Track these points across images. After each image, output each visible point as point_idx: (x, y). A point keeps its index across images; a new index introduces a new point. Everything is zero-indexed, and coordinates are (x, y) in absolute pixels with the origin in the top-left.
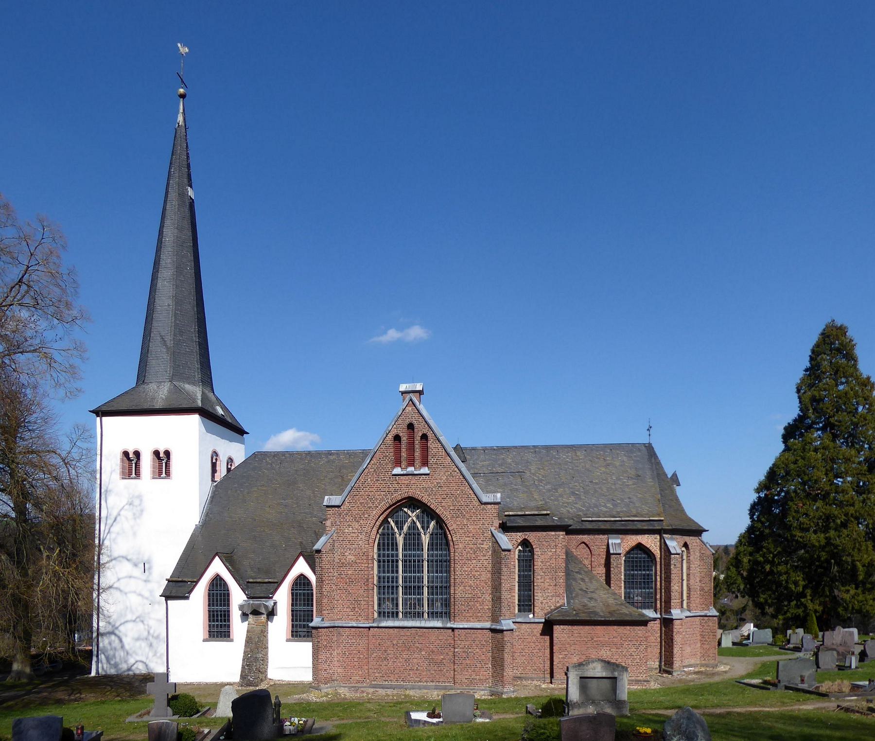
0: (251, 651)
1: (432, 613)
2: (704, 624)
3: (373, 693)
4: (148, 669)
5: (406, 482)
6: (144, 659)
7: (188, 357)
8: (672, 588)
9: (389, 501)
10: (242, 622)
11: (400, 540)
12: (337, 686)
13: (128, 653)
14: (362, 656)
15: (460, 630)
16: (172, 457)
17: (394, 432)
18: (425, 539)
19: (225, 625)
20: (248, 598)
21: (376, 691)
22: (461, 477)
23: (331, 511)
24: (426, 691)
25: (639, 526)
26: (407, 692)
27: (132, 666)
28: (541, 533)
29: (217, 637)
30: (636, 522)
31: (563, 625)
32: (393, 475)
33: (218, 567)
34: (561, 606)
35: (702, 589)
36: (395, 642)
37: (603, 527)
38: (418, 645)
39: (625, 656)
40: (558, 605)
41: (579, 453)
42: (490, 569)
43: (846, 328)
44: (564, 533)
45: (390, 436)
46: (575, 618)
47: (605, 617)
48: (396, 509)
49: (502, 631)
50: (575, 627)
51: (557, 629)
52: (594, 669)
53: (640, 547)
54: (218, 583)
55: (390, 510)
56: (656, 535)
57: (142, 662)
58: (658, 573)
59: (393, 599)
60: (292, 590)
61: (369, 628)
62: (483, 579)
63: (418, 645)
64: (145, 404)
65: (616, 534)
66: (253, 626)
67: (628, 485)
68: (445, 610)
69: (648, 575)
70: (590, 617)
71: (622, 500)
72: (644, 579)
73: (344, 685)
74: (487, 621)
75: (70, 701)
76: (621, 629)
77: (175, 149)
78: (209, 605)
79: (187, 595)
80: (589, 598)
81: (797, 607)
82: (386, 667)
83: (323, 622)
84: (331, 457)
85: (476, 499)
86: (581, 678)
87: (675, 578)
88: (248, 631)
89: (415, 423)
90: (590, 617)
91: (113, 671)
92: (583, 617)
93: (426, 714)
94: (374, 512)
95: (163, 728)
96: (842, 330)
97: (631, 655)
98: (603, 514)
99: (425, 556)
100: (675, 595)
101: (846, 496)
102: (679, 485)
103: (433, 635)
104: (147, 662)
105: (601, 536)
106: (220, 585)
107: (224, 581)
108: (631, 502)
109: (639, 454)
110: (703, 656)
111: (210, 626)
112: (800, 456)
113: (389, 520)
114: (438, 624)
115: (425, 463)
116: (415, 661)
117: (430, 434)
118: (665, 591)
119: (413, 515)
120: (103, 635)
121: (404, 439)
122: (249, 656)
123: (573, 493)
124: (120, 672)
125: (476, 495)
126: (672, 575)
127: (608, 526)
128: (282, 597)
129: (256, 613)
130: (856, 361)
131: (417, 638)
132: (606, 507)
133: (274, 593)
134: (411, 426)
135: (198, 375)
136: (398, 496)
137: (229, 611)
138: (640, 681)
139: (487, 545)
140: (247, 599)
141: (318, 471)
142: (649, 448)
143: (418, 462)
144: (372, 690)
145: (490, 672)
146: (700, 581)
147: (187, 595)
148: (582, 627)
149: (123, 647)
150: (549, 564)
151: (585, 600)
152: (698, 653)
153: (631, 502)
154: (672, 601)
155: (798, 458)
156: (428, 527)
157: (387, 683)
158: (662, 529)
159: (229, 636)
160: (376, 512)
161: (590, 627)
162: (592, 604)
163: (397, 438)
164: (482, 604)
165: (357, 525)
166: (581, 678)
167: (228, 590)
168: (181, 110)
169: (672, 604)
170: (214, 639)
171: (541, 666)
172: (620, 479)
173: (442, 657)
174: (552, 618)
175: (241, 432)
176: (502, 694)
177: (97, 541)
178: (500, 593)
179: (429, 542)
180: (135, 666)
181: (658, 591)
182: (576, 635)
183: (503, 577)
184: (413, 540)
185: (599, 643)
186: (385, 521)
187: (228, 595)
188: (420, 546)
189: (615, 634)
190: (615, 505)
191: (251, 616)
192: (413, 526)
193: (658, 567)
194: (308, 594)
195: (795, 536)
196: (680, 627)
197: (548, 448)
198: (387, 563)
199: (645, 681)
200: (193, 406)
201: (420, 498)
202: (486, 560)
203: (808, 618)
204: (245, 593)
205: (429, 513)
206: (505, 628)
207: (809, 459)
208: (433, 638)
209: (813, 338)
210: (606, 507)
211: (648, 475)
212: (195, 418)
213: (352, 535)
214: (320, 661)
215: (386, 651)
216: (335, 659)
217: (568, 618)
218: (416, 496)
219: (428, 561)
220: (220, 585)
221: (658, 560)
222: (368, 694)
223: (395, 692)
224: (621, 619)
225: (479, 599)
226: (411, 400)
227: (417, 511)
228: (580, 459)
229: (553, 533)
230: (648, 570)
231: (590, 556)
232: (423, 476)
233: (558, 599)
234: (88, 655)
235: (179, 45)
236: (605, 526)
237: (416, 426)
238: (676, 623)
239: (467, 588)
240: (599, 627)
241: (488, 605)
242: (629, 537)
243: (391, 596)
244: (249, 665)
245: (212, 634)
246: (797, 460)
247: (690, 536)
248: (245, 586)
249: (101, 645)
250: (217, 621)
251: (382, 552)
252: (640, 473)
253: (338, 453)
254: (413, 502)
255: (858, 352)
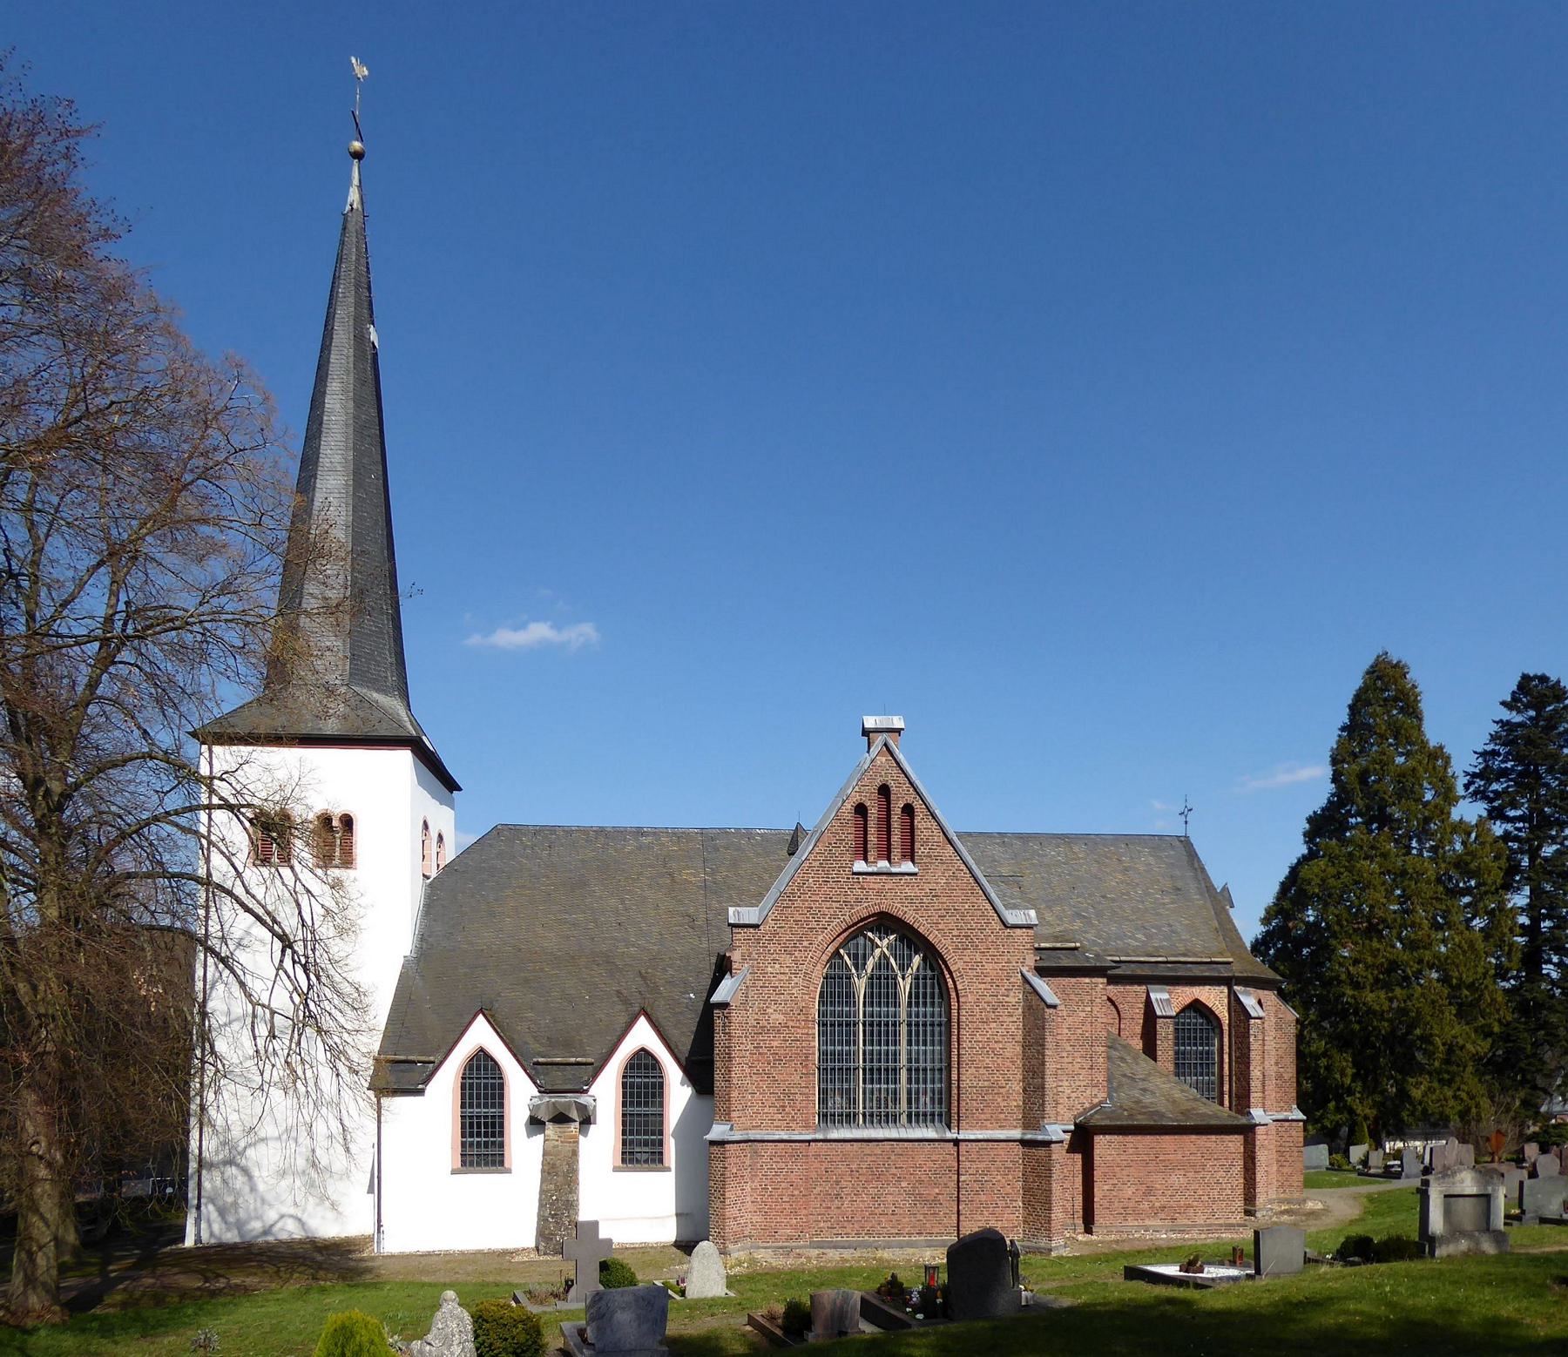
0: (558, 1189)
1: (825, 1115)
2: (1283, 1134)
3: (818, 1257)
4: (305, 1230)
5: (876, 886)
6: (292, 1211)
7: (374, 641)
8: (1252, 1074)
9: (847, 918)
10: (530, 1134)
11: (861, 985)
12: (751, 1247)
13: (263, 1201)
14: (796, 1192)
15: (969, 1144)
16: (358, 827)
17: (856, 799)
18: (905, 986)
19: (493, 1143)
20: (540, 1092)
21: (823, 1254)
22: (972, 880)
23: (741, 935)
24: (911, 1251)
25: (1197, 971)
26: (879, 1254)
27: (272, 1226)
28: (1067, 979)
29: (479, 1164)
30: (1189, 966)
31: (1110, 1134)
32: (854, 874)
33: (481, 1035)
34: (1101, 1102)
35: (1279, 1077)
36: (854, 1167)
37: (1139, 972)
38: (894, 1171)
39: (1208, 1184)
40: (1096, 1101)
41: (1076, 849)
42: (1019, 1038)
43: (1405, 666)
44: (1105, 980)
45: (849, 806)
46: (1130, 1123)
47: (1177, 1121)
48: (856, 931)
49: (1048, 1144)
50: (1130, 1138)
51: (1100, 1142)
52: (1462, 1181)
53: (1196, 1007)
54: (482, 1063)
55: (845, 934)
56: (1222, 987)
57: (291, 1216)
58: (1226, 1049)
59: (848, 1090)
60: (624, 1077)
61: (809, 1141)
62: (1008, 1055)
63: (894, 1171)
64: (303, 725)
65: (1159, 984)
66: (556, 1143)
67: (1164, 904)
68: (946, 1110)
69: (1208, 1053)
70: (1155, 1121)
71: (1159, 928)
72: (1201, 1059)
73: (765, 1245)
74: (1016, 1127)
75: (214, 1294)
76: (1202, 1141)
77: (345, 252)
78: (463, 1106)
79: (420, 1086)
80: (1141, 1089)
81: (1338, 1110)
82: (839, 1211)
83: (732, 1133)
84: (644, 840)
85: (996, 918)
86: (1445, 1196)
87: (1255, 1055)
88: (545, 1154)
89: (892, 784)
90: (1155, 1121)
91: (231, 1237)
92: (1142, 1120)
93: (1178, 1268)
94: (820, 938)
95: (838, 1302)
96: (1399, 670)
97: (1218, 1183)
98: (1133, 950)
99: (903, 1016)
100: (1255, 1084)
101: (1420, 933)
102: (1232, 906)
103: (922, 1154)
104: (304, 1218)
105: (1136, 988)
106: (486, 1069)
107: (493, 1059)
108: (1172, 931)
109: (1172, 853)
110: (1282, 1186)
111: (463, 1145)
112: (1346, 867)
113: (842, 951)
114: (930, 1133)
115: (910, 855)
116: (890, 1198)
117: (917, 805)
118: (1238, 1079)
119: (884, 943)
120: (211, 1166)
121: (873, 813)
122: (554, 1198)
123: (1078, 915)
124: (248, 1238)
125: (996, 912)
126: (1252, 1053)
127: (1146, 971)
128: (606, 1093)
129: (561, 1118)
130: (1420, 720)
131: (893, 1157)
132: (1136, 939)
133: (590, 1083)
134: (884, 790)
135: (392, 676)
136: (862, 910)
137: (502, 1117)
138: (1233, 1225)
139: (1016, 997)
140: (538, 1094)
141: (624, 864)
142: (1186, 842)
143: (896, 853)
144: (817, 1252)
145: (1020, 1214)
146: (1277, 1064)
147: (420, 1086)
148: (1139, 1137)
149: (253, 1189)
150: (1080, 1031)
151: (1136, 1093)
152: (1274, 1181)
153: (1172, 931)
154: (1252, 1095)
155: (1342, 870)
156: (909, 965)
157: (839, 1239)
158: (1234, 977)
159: (502, 1163)
160: (822, 942)
161: (1152, 1137)
162: (1148, 1099)
163: (861, 810)
164: (1007, 1097)
165: (788, 960)
166: (1445, 1196)
167: (502, 1078)
168: (356, 182)
169: (1252, 1100)
170: (472, 1168)
171: (1069, 1205)
172: (1148, 894)
173: (937, 1191)
174: (1093, 1122)
175: (451, 785)
176: (1051, 1250)
177: (199, 985)
178: (1043, 1078)
179: (910, 993)
180: (279, 1225)
181: (1226, 1079)
182: (1131, 1151)
183: (1047, 1052)
184: (883, 987)
185: (1167, 1163)
186: (836, 954)
187: (502, 1086)
188: (850, 997)
189: (1193, 1148)
190: (1150, 937)
191: (549, 1126)
192: (883, 963)
193: (1226, 1040)
194: (654, 1084)
195: (1344, 994)
196: (1265, 1137)
197: (1024, 838)
198: (835, 1027)
199: (1239, 1225)
200: (401, 733)
201: (901, 914)
202: (1013, 1023)
203: (1356, 1128)
204: (535, 1083)
205: (911, 939)
206: (1054, 1139)
207: (1360, 873)
208: (920, 1160)
209: (1353, 682)
210: (1136, 939)
211: (1192, 887)
212: (405, 757)
213: (780, 976)
214: (727, 1202)
215: (837, 1183)
216: (748, 1198)
217: (1119, 1123)
218: (894, 912)
219: (864, 1025)
220: (486, 1069)
221: (1226, 1028)
222: (809, 1259)
223: (857, 1254)
224: (1204, 1123)
225: (1001, 1090)
226: (886, 745)
227: (892, 937)
228: (1079, 859)
229: (1087, 980)
230: (1207, 1045)
231: (1117, 1021)
232: (907, 877)
233: (1095, 1091)
234: (177, 1202)
235: (354, 60)
236: (1143, 971)
237: (894, 789)
238: (1259, 1130)
239: (982, 1071)
240: (1167, 1137)
241: (1017, 1100)
242: (1179, 989)
243: (845, 1086)
244: (555, 1214)
245: (468, 1158)
246: (1339, 873)
247: (1263, 989)
248: (534, 1070)
249: (206, 1185)
250: (479, 1135)
251: (914, 1009)
252: (1179, 884)
253: (656, 833)
254: (885, 922)
255: (1425, 706)
